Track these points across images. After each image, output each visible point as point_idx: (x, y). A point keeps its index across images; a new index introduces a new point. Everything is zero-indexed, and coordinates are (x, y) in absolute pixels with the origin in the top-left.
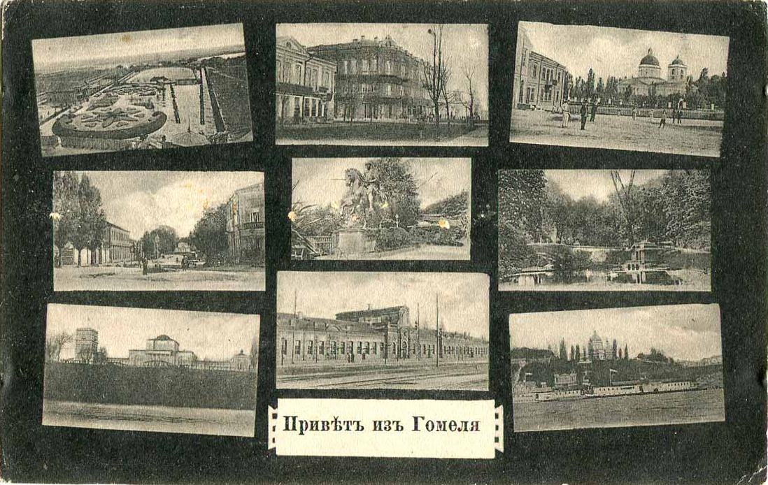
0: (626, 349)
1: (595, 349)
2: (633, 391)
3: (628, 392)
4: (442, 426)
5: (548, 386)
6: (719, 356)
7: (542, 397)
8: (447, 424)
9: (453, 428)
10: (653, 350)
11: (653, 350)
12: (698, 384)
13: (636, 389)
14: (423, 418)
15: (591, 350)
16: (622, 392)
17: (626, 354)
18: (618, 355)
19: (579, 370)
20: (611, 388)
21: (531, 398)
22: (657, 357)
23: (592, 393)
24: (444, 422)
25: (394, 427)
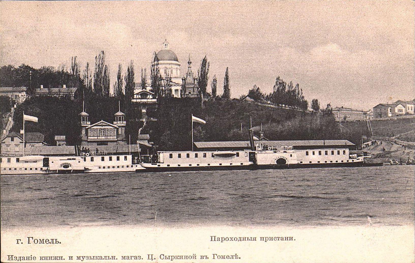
0: (227, 79)
1: (164, 76)
2: (236, 162)
3: (226, 163)
4: (42, 241)
5: (69, 142)
6: (408, 103)
7: (56, 164)
8: (44, 241)
9: (47, 242)
10: (281, 84)
11: (281, 84)
12: (365, 154)
13: (243, 159)
14: (32, 238)
15: (156, 78)
16: (215, 163)
17: (226, 88)
18: (209, 90)
19: (132, 111)
20: (192, 154)
21: (33, 165)
22: (286, 97)
23: (155, 160)
24: (43, 240)
25: (205, 258)
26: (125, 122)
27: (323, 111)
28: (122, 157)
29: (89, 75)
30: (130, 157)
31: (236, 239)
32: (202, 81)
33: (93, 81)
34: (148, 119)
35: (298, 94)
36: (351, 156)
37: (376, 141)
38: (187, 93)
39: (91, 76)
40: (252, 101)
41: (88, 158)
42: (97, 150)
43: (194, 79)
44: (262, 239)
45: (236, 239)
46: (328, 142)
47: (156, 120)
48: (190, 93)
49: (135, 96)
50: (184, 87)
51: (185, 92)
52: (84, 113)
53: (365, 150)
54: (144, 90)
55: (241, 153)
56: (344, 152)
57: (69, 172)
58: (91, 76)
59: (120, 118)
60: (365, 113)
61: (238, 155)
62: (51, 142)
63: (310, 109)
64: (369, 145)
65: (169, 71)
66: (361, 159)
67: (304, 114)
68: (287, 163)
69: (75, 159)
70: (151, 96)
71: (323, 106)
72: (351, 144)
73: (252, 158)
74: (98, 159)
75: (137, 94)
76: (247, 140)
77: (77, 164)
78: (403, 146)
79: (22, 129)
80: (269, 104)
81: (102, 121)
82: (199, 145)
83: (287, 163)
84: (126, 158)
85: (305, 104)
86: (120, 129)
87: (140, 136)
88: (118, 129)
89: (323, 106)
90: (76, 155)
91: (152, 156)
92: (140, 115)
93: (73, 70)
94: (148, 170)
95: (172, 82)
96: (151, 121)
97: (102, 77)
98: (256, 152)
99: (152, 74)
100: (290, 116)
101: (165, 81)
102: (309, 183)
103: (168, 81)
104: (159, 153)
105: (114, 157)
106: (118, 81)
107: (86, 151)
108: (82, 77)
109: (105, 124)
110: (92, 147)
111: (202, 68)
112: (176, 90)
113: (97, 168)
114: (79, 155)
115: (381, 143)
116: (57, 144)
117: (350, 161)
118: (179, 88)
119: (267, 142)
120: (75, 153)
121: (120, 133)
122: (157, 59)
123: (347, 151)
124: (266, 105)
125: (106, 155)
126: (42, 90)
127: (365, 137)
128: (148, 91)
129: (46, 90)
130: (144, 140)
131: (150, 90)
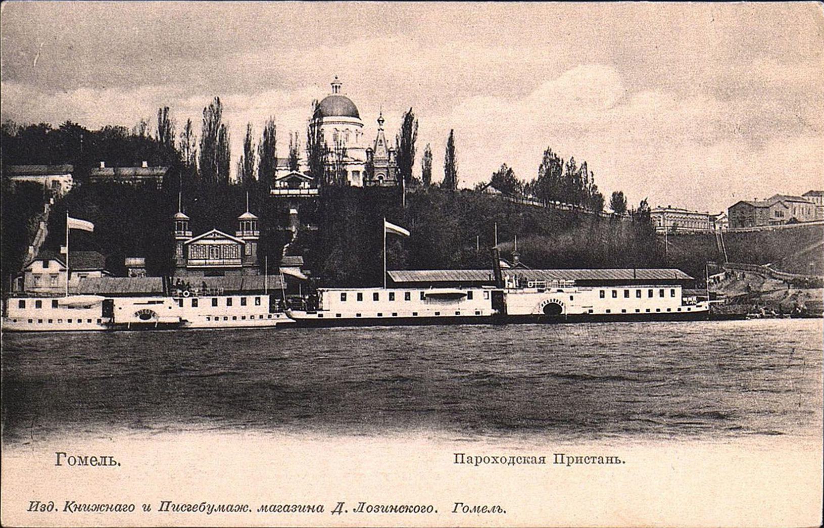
1: (331, 145)
2: (467, 308)
3: (448, 310)
9: (94, 463)
12: (713, 296)
13: (480, 303)
18: (417, 171)
19: (272, 212)
20: (384, 293)
21: (83, 314)
26: (257, 233)
27: (632, 213)
28: (251, 299)
29: (191, 144)
30: (265, 299)
31: (503, 460)
35: (586, 181)
36: (685, 299)
37: (733, 272)
40: (498, 194)
41: (188, 301)
42: (205, 286)
43: (390, 152)
44: (131, 508)
45: (503, 460)
48: (381, 178)
49: (278, 184)
50: (370, 169)
51: (372, 176)
53: (713, 289)
54: (294, 172)
60: (713, 218)
61: (470, 296)
62: (117, 269)
63: (608, 209)
64: (721, 278)
65: (341, 136)
66: (705, 306)
67: (598, 218)
68: (563, 313)
69: (162, 302)
71: (632, 204)
72: (680, 274)
73: (498, 301)
77: (167, 311)
78: (785, 281)
79: (65, 246)
80: (530, 200)
83: (563, 313)
86: (248, 247)
87: (285, 259)
88: (243, 246)
89: (632, 204)
90: (164, 294)
92: (286, 219)
93: (161, 134)
94: (300, 323)
95: (347, 156)
96: (307, 230)
99: (309, 142)
100: (571, 221)
102: (605, 352)
103: (339, 154)
104: (322, 292)
105: (236, 299)
107: (182, 287)
110: (195, 280)
113: (205, 319)
114: (170, 295)
115: (744, 276)
117: (684, 309)
118: (361, 168)
119: (527, 273)
122: (319, 113)
124: (525, 202)
126: (105, 170)
127: (712, 265)
129: (111, 171)
131: (305, 173)
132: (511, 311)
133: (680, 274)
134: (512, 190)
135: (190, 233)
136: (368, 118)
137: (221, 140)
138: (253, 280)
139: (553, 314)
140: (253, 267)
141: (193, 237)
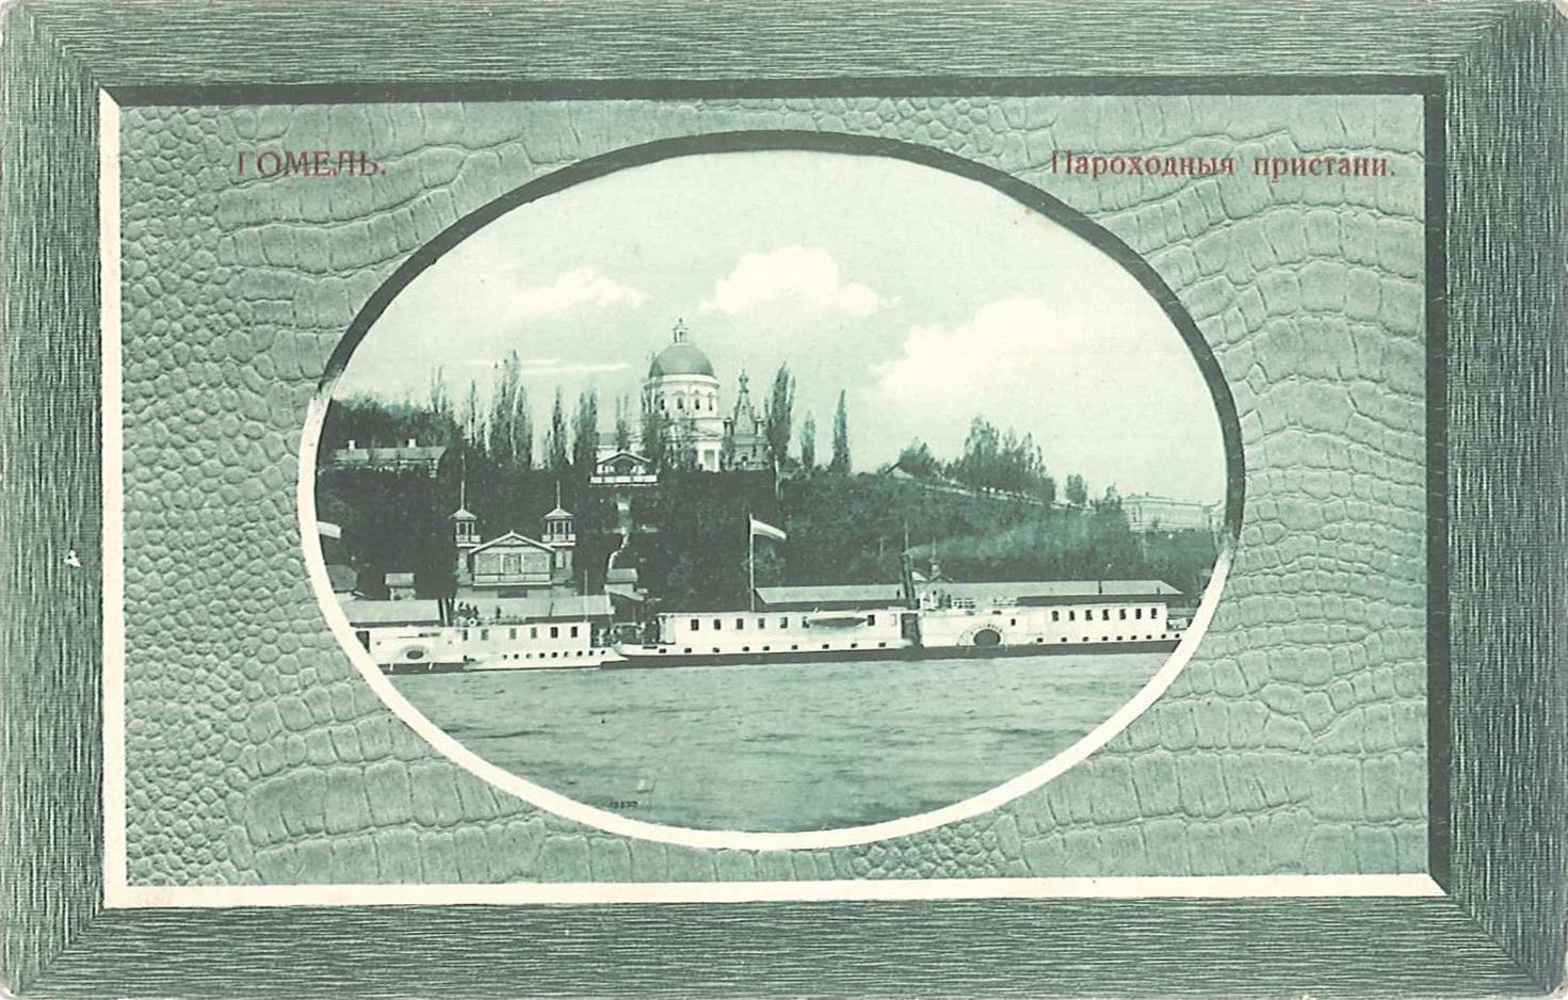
2: (867, 638)
3: (840, 641)
13: (886, 630)
18: (795, 450)
19: (591, 514)
20: (750, 619)
22: (1001, 472)
27: (1097, 505)
28: (565, 629)
30: (584, 629)
32: (777, 428)
33: (488, 429)
34: (634, 526)
35: (1031, 459)
38: (738, 459)
39: (481, 416)
41: (474, 632)
42: (499, 611)
43: (756, 424)
46: (1061, 588)
47: (654, 530)
48: (745, 459)
49: (600, 470)
50: (730, 445)
52: (462, 514)
55: (878, 614)
56: (1154, 612)
57: (423, 669)
58: (481, 416)
59: (560, 525)
63: (1062, 499)
67: (1048, 512)
68: (1001, 643)
70: (640, 468)
71: (1096, 492)
72: (1167, 589)
73: (910, 627)
74: (500, 633)
75: (605, 463)
76: (897, 582)
77: (446, 646)
80: (954, 486)
81: (512, 534)
82: (769, 595)
84: (574, 632)
85: (1048, 488)
87: (612, 573)
89: (1096, 492)
90: (441, 624)
91: (643, 625)
92: (614, 518)
93: (435, 400)
94: (633, 662)
97: (510, 423)
98: (920, 614)
100: (1015, 515)
101: (679, 429)
103: (686, 427)
104: (664, 618)
106: (556, 428)
107: (470, 613)
108: (458, 421)
109: (519, 542)
110: (486, 604)
111: (775, 394)
112: (709, 453)
114: (451, 625)
116: (392, 596)
118: (717, 447)
119: (949, 588)
120: (438, 618)
121: (559, 564)
122: (657, 371)
123: (1162, 610)
124: (947, 489)
125: (521, 623)
128: (633, 454)
129: (364, 455)
130: (624, 583)
131: (638, 453)
132: (927, 642)
133: (1167, 589)
134: (928, 473)
135: (477, 538)
136: (727, 376)
137: (520, 406)
138: (569, 603)
139: (987, 645)
140: (566, 585)
141: (482, 542)
